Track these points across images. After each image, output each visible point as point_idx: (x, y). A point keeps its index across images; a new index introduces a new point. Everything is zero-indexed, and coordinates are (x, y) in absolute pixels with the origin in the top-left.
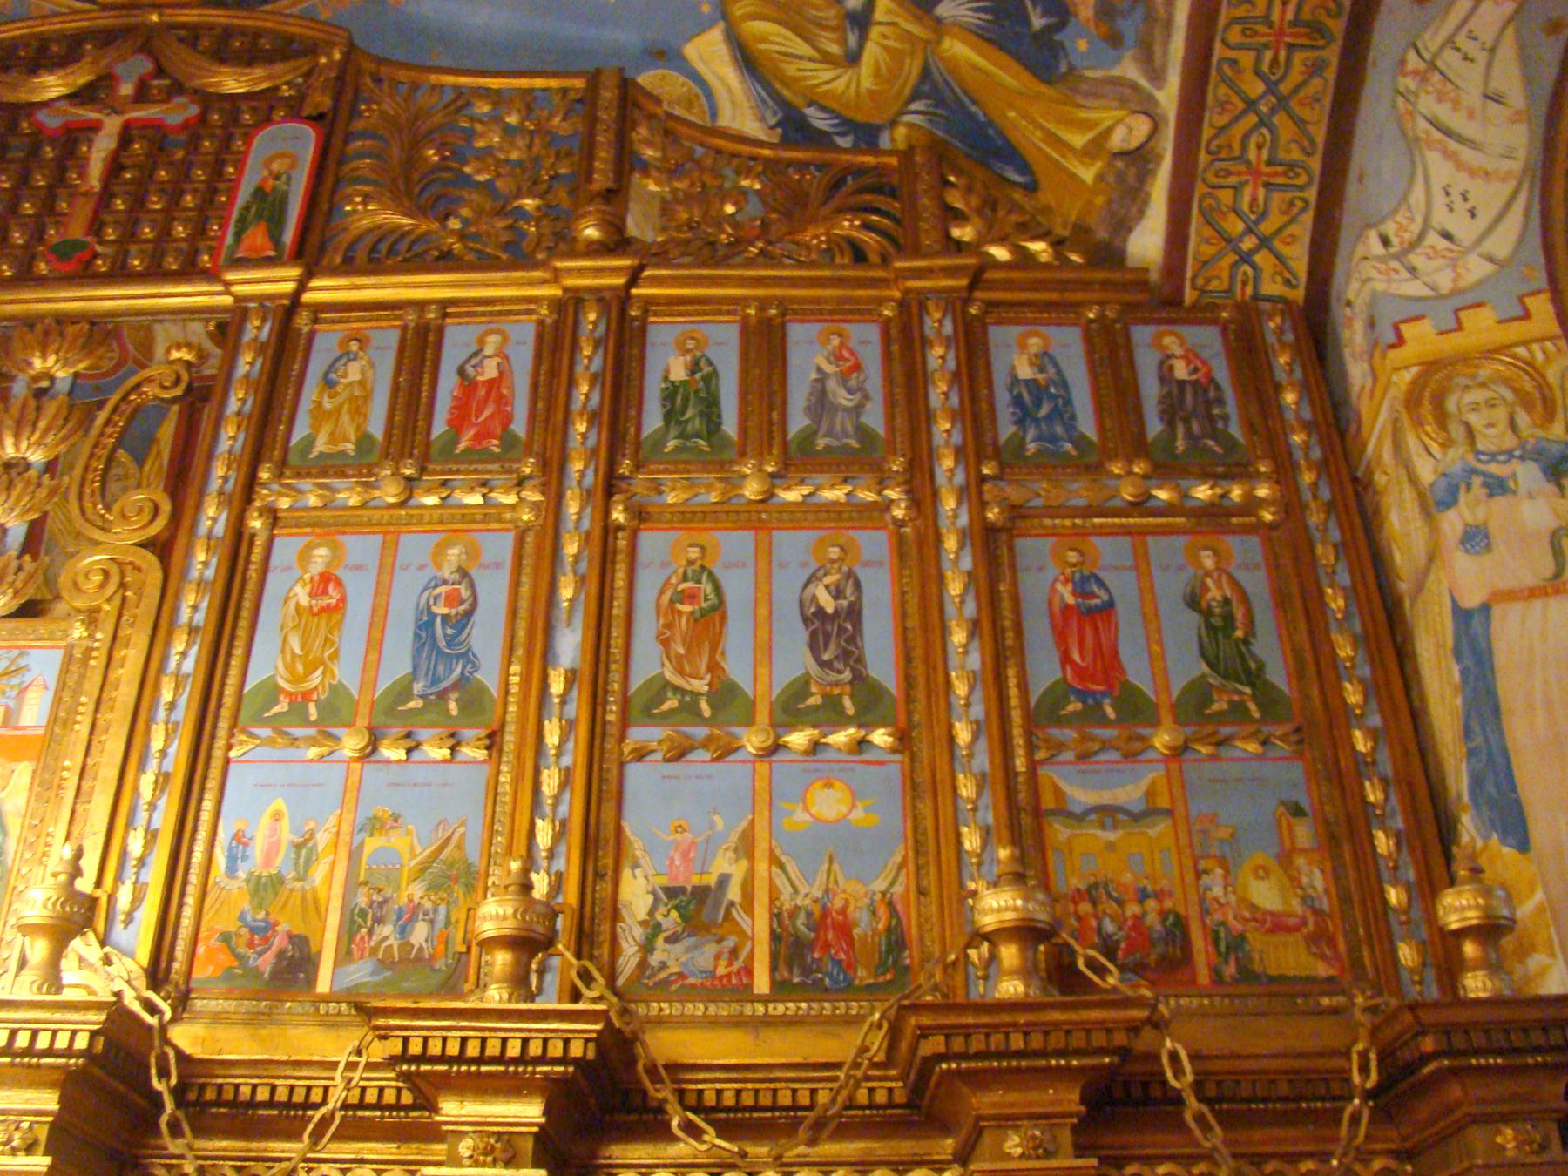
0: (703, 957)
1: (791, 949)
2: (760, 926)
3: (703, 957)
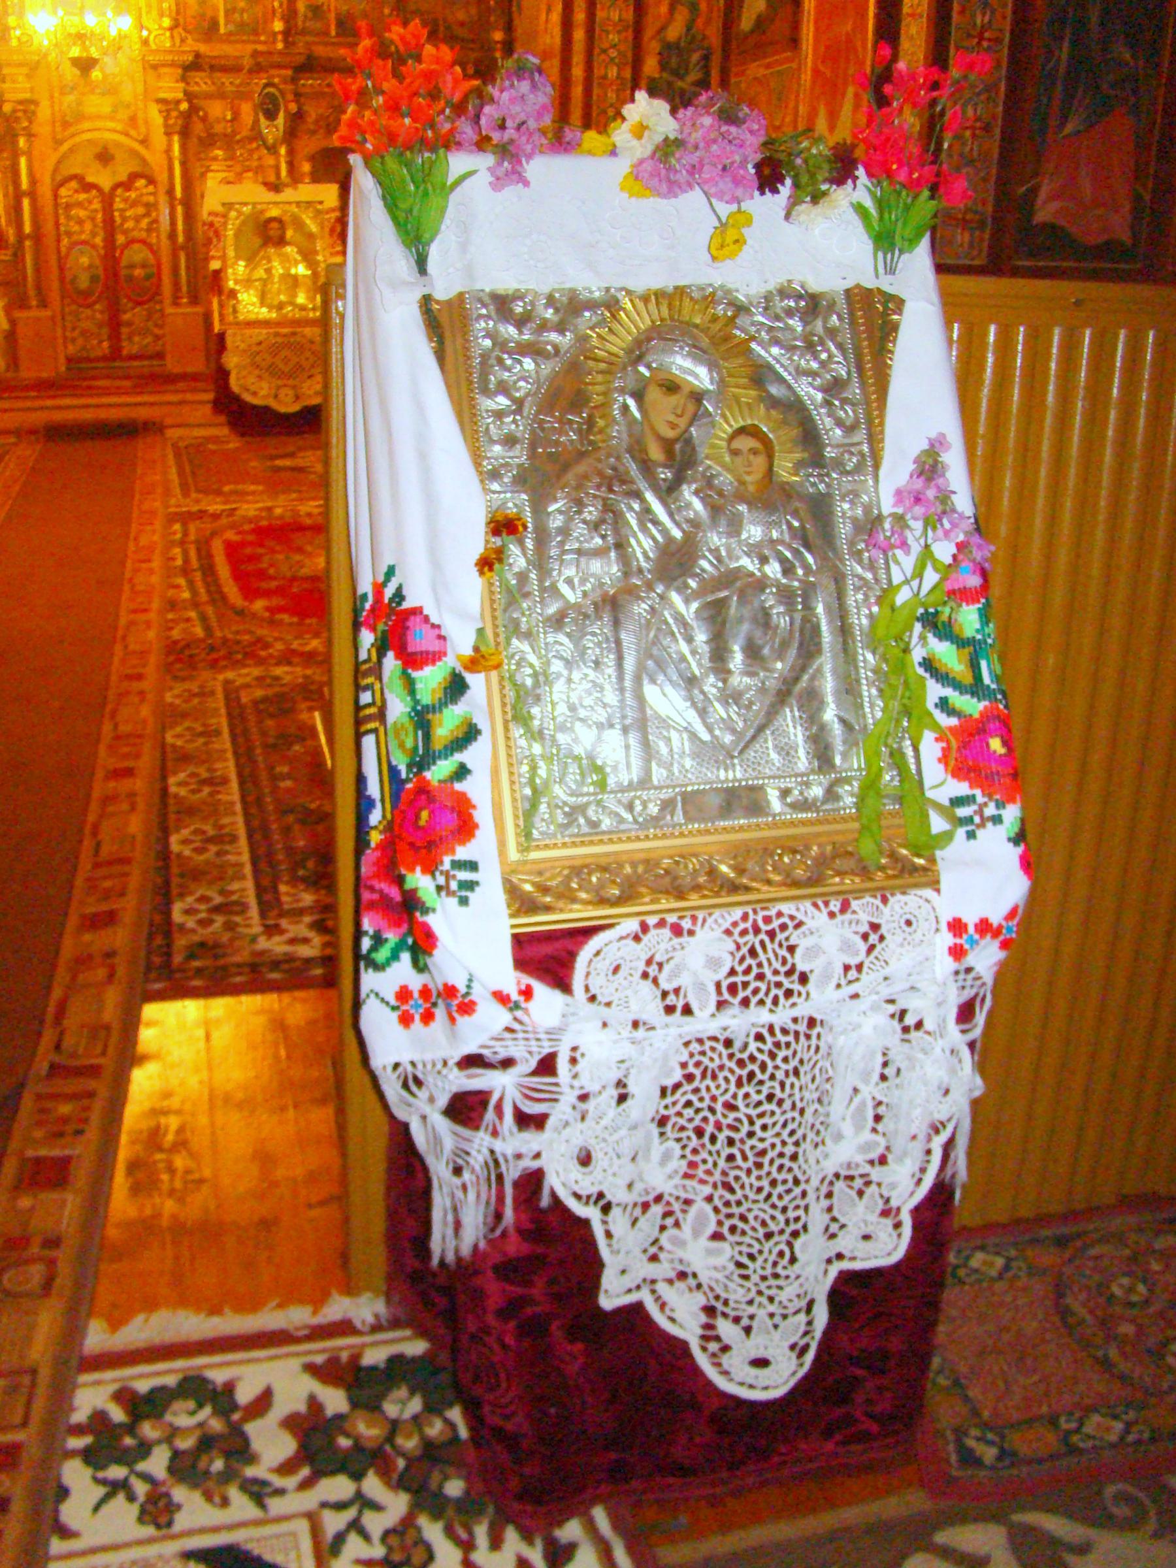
0: (318, 25)
1: (340, 24)
2: (332, 16)
3: (318, 25)
